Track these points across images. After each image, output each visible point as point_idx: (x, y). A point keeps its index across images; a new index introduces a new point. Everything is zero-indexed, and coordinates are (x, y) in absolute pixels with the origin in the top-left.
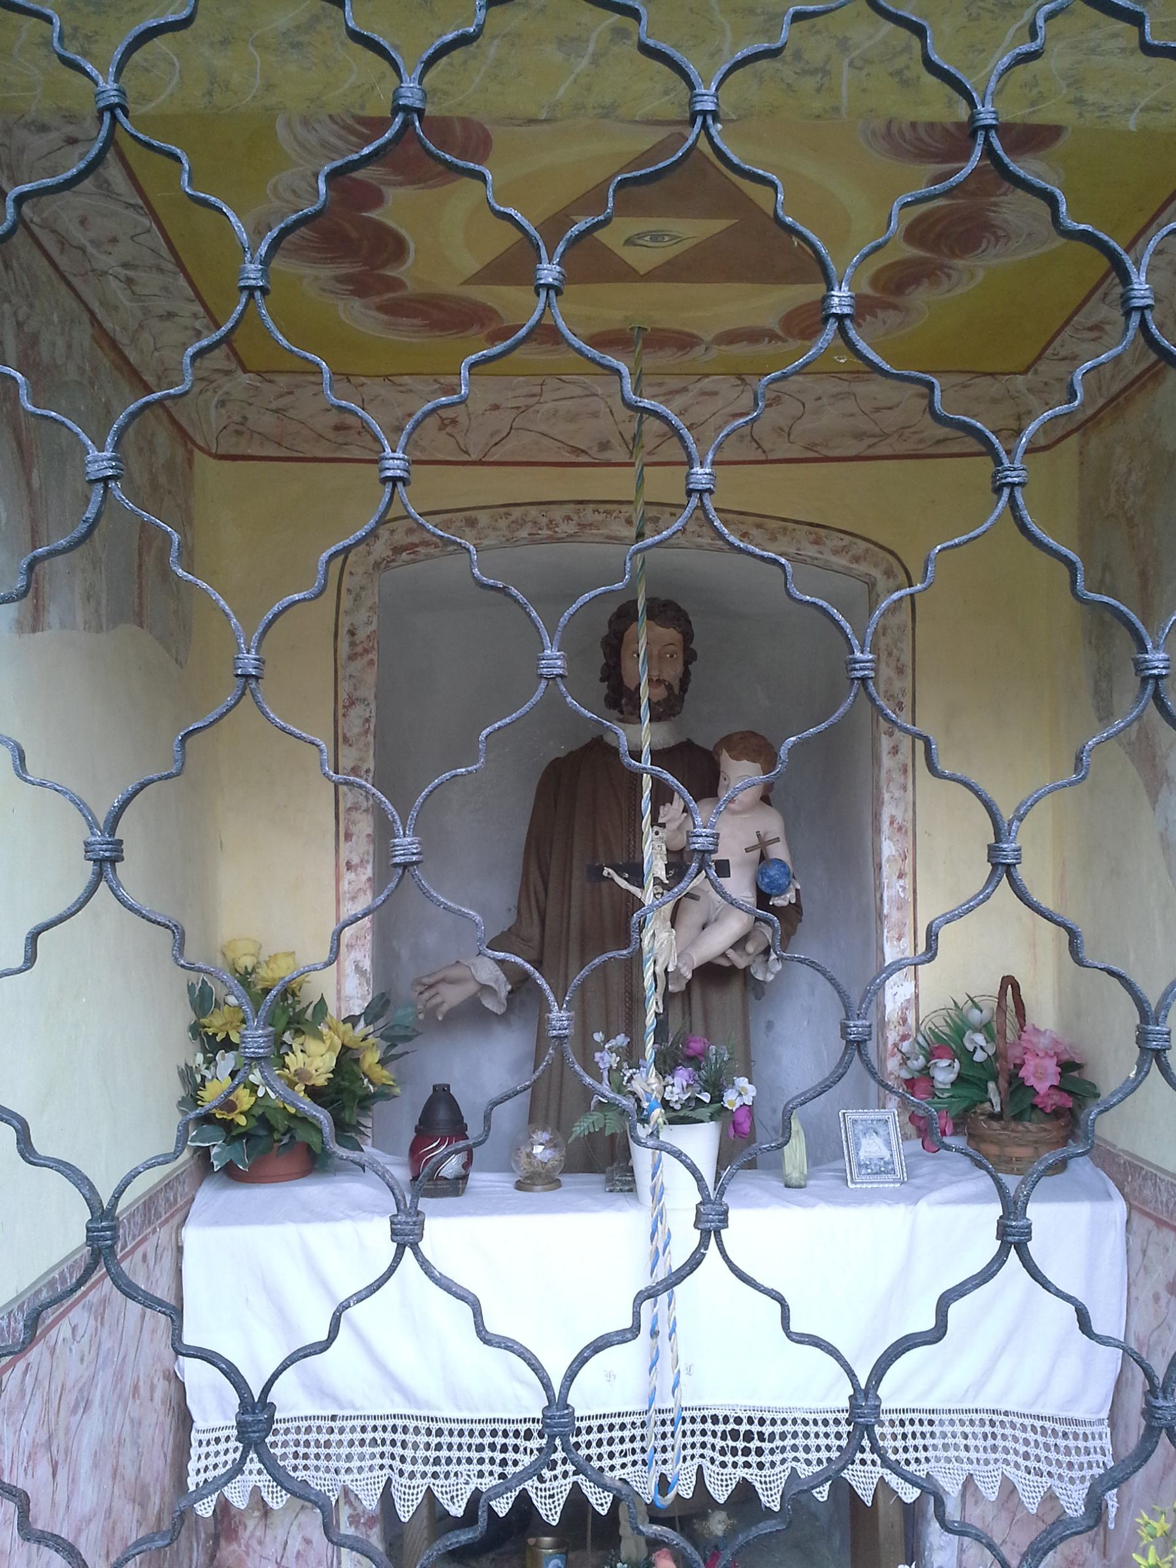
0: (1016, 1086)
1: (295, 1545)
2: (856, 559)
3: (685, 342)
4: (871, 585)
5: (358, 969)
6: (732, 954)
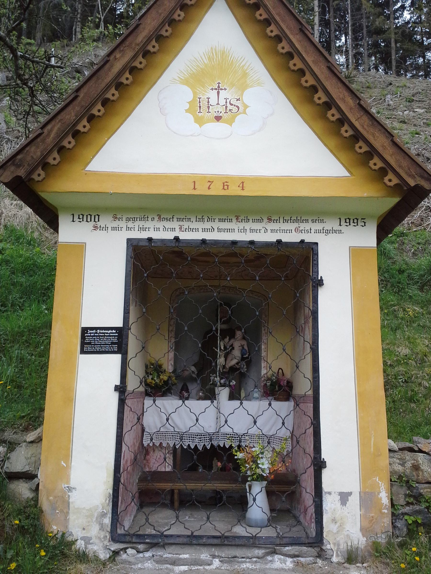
0: (280, 386)
1: (158, 457)
2: (259, 297)
3: (228, 263)
4: (262, 301)
5: (171, 364)
6: (236, 365)
